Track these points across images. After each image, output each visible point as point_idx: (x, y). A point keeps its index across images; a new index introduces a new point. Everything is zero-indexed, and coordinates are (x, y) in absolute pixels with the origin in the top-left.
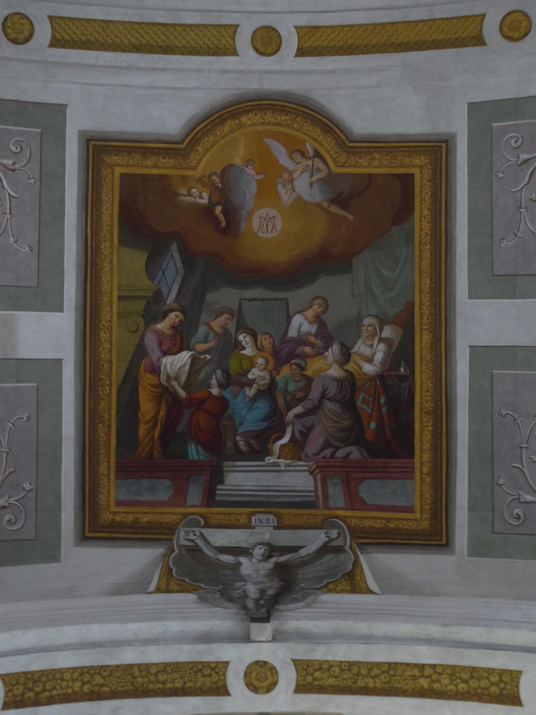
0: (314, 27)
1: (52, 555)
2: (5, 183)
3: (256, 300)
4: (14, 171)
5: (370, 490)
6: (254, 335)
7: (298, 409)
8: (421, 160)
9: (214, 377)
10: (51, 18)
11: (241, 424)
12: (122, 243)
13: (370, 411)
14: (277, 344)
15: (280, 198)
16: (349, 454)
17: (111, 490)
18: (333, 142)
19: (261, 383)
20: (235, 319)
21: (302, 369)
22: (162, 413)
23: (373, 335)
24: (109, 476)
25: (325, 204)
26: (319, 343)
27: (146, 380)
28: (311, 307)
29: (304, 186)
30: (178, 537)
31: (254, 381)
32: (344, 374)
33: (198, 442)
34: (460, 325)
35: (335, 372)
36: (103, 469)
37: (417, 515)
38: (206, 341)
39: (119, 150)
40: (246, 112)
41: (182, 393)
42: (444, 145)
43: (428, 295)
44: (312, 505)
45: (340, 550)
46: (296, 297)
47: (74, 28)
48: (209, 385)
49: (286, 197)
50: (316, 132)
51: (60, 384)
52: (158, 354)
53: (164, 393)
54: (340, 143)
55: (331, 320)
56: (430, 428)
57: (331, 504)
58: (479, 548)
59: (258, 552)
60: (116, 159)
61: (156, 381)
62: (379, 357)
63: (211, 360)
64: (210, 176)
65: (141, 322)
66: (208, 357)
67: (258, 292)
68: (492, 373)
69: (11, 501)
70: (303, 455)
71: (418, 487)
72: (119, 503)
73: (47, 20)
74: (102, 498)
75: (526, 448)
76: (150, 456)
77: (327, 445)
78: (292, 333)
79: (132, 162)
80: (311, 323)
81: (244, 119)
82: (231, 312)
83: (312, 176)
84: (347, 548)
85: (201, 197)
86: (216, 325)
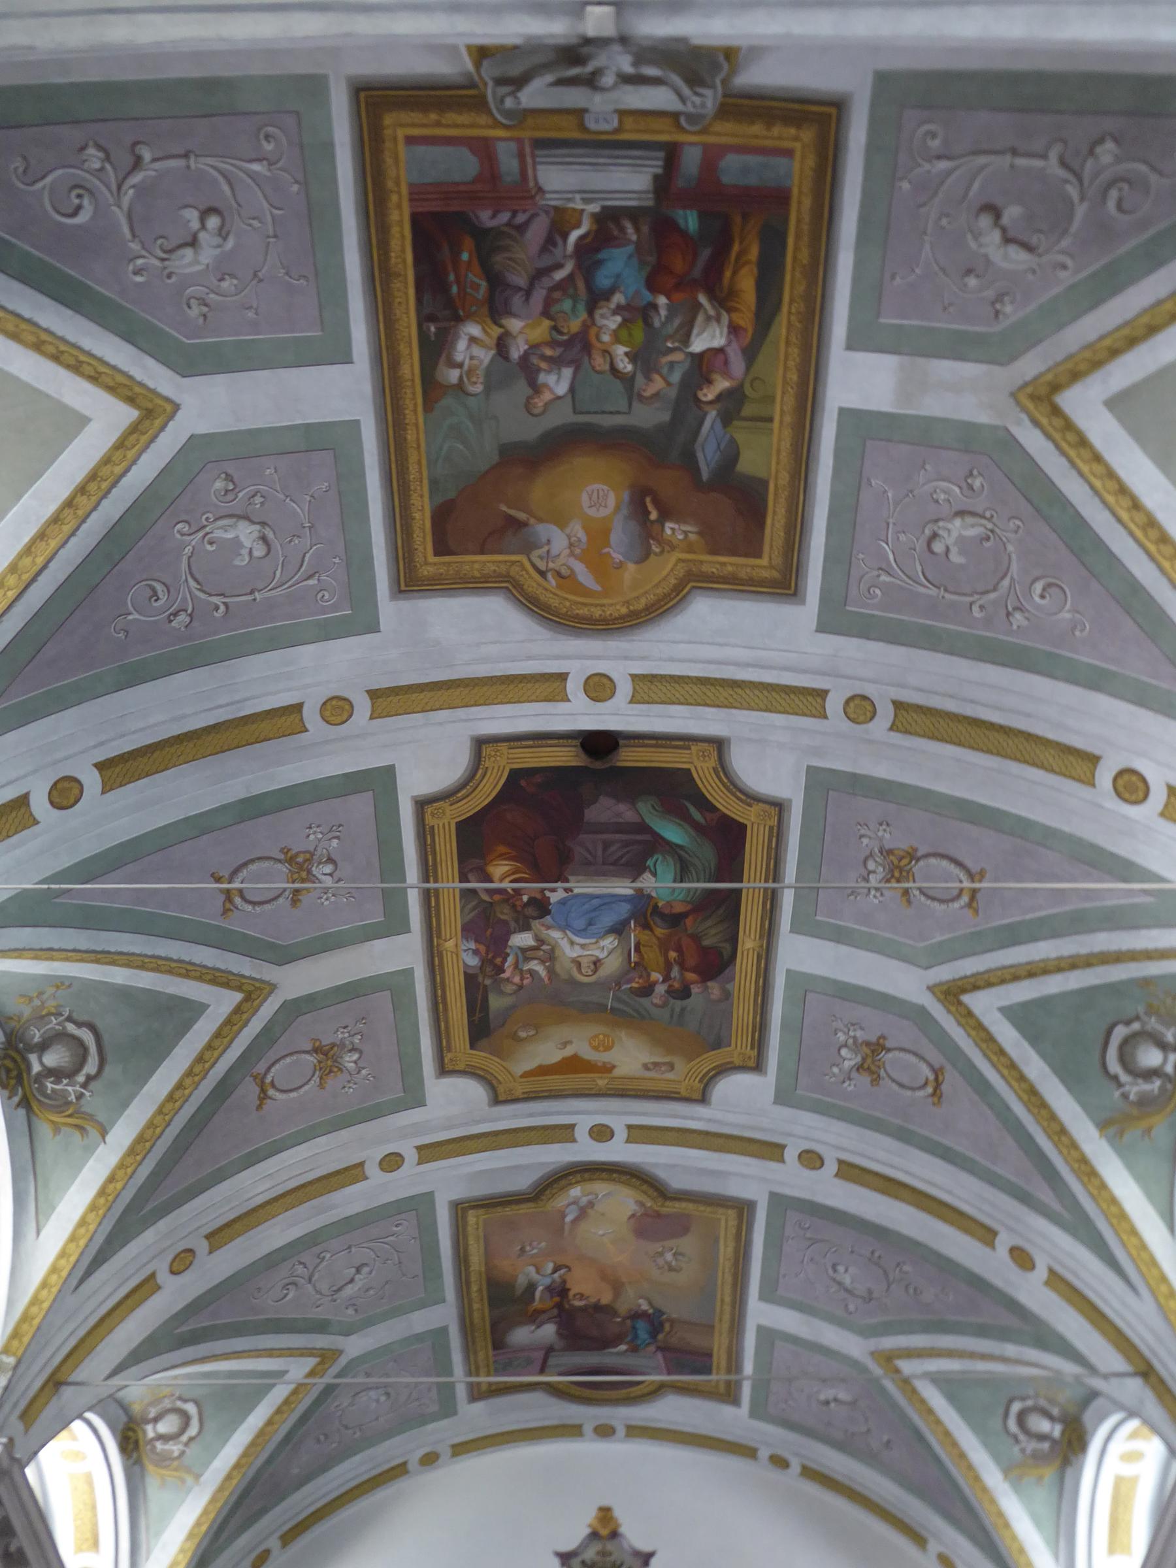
0: (550, 701)
1: (884, 81)
2: (891, 557)
3: (611, 413)
4: (881, 569)
5: (462, 166)
6: (614, 370)
7: (559, 275)
8: (426, 571)
9: (663, 319)
10: (825, 717)
11: (630, 257)
12: (764, 483)
13: (470, 275)
14: (586, 358)
15: (583, 528)
16: (494, 216)
17: (797, 173)
18: (525, 587)
19: (604, 311)
20: (636, 390)
21: (555, 328)
22: (728, 274)
23: (470, 372)
24: (800, 192)
25: (532, 521)
26: (535, 360)
27: (746, 319)
28: (546, 404)
29: (557, 542)
30: (715, 98)
31: (615, 312)
32: (504, 322)
33: (684, 234)
34: (367, 388)
35: (515, 325)
36: (807, 202)
37: (401, 133)
38: (672, 365)
39: (762, 583)
40: (622, 618)
41: (702, 299)
42: (403, 588)
43: (407, 421)
44: (541, 144)
45: (500, 81)
46: (563, 416)
47: (801, 706)
48: (671, 309)
49: (577, 530)
50: (544, 597)
51: (851, 318)
52: (729, 350)
53: (725, 300)
54: (518, 586)
55: (521, 388)
56: (393, 254)
57: (513, 146)
58: (312, 87)
59: (608, 80)
60: (766, 574)
61: (735, 316)
62: (462, 345)
63: (666, 341)
64: (662, 552)
65: (748, 390)
66: (669, 345)
67: (607, 421)
68: (322, 330)
69: (927, 166)
70: (552, 212)
71: (402, 173)
72: (789, 153)
73: (829, 715)
74: (811, 162)
75: (268, 237)
76: (745, 217)
77: (522, 228)
78: (567, 372)
79: (749, 570)
80: (546, 385)
81: (624, 610)
82: (641, 398)
83: (548, 552)
84: (490, 84)
85: (672, 529)
86: (658, 384)
